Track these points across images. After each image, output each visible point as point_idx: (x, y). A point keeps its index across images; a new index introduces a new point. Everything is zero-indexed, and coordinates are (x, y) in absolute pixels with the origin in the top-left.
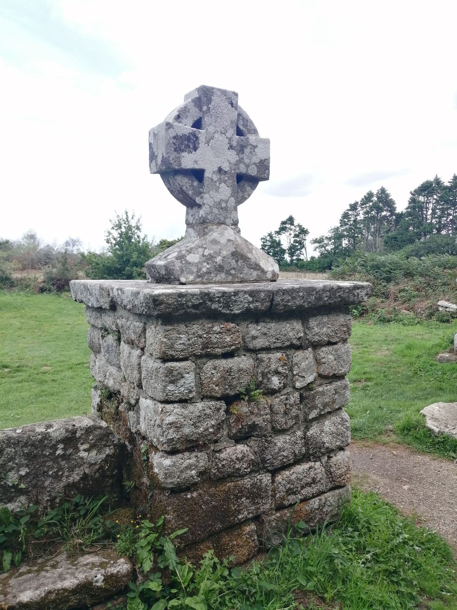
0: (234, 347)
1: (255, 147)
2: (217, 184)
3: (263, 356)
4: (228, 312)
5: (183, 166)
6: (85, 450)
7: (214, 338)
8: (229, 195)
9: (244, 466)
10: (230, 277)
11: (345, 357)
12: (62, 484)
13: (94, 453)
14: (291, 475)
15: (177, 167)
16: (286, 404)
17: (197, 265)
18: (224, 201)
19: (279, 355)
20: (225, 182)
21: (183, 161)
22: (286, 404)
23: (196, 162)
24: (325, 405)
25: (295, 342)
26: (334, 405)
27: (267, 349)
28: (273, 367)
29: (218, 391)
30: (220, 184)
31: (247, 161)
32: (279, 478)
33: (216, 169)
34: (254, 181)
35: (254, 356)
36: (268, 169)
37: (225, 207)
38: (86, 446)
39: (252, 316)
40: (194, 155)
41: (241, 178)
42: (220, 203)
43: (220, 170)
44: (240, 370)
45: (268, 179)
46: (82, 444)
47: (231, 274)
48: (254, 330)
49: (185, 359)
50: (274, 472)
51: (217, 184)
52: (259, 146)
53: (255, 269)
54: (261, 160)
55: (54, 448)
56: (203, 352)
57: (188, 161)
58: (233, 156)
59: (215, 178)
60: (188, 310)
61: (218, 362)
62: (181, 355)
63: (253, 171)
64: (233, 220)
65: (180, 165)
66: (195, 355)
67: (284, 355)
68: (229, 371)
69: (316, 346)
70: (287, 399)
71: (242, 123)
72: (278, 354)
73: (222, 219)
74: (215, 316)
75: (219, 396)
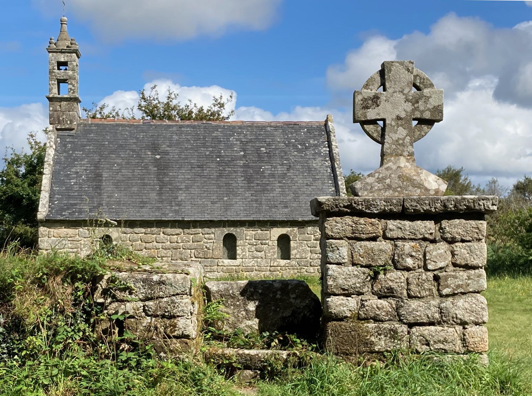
0: (374, 234)
1: (429, 98)
2: (396, 128)
3: (400, 243)
4: (369, 211)
5: (369, 118)
6: (293, 298)
7: (360, 228)
8: (405, 135)
9: (383, 314)
10: (397, 193)
11: (478, 253)
12: (279, 316)
13: (298, 301)
14: (424, 330)
15: (363, 119)
16: (419, 279)
17: (371, 184)
18: (401, 139)
19: (413, 244)
20: (401, 125)
21: (368, 114)
22: (419, 279)
23: (378, 114)
24: (458, 286)
25: (427, 236)
26: (468, 287)
27: (403, 239)
28: (406, 252)
29: (364, 262)
30: (398, 127)
31: (422, 108)
32: (414, 330)
33: (394, 117)
34: (430, 123)
35: (392, 242)
36: (442, 113)
37: (402, 143)
38: (294, 296)
39: (385, 215)
40: (376, 110)
41: (422, 121)
42: (397, 141)
43: (399, 118)
44: (381, 250)
45: (442, 120)
46: (292, 294)
47: (397, 191)
48: (392, 224)
49: (341, 239)
50: (411, 325)
51: (396, 128)
52: (433, 96)
53: (419, 188)
54: (434, 107)
55: (275, 293)
56: (353, 236)
57: (371, 114)
58: (409, 107)
59: (393, 123)
60: (341, 209)
61: (363, 243)
62: (337, 236)
63: (427, 115)
64: (409, 152)
65: (366, 117)
66: (347, 237)
67: (418, 244)
68: (372, 250)
69: (452, 241)
70: (419, 275)
71: (419, 81)
72: (412, 243)
73: (400, 152)
74: (361, 214)
75: (364, 265)
